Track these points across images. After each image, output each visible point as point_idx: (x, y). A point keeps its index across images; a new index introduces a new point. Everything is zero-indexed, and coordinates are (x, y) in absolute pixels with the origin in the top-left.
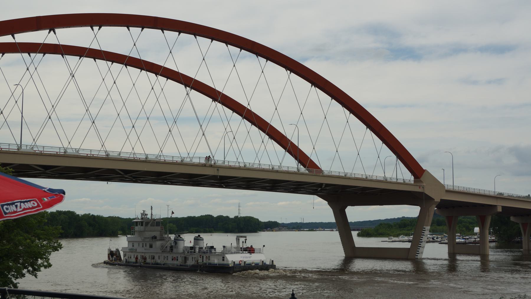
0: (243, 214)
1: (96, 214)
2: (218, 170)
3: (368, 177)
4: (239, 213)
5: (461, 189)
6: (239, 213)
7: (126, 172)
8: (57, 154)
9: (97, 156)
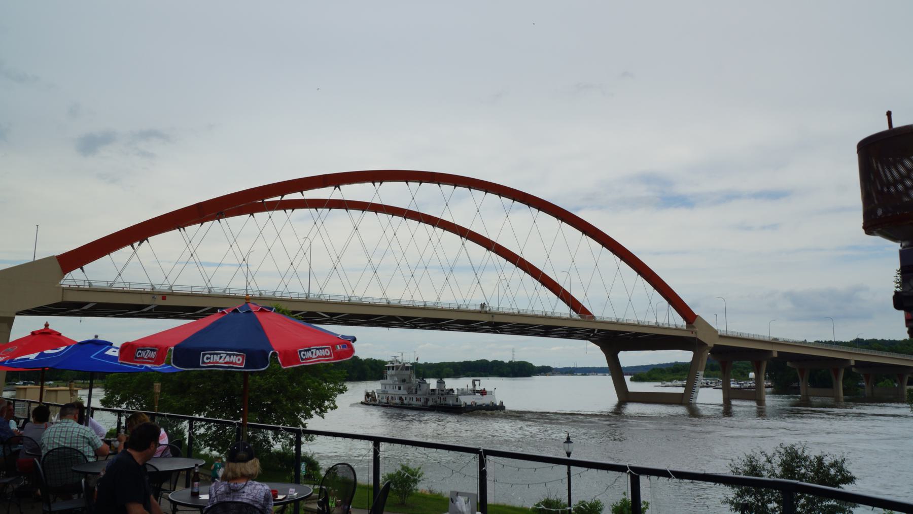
0: (517, 359)
1: (377, 359)
2: (493, 316)
3: (264, 294)
4: (513, 358)
5: (735, 335)
6: (513, 358)
7: (406, 318)
8: (123, 290)
9: (241, 295)
